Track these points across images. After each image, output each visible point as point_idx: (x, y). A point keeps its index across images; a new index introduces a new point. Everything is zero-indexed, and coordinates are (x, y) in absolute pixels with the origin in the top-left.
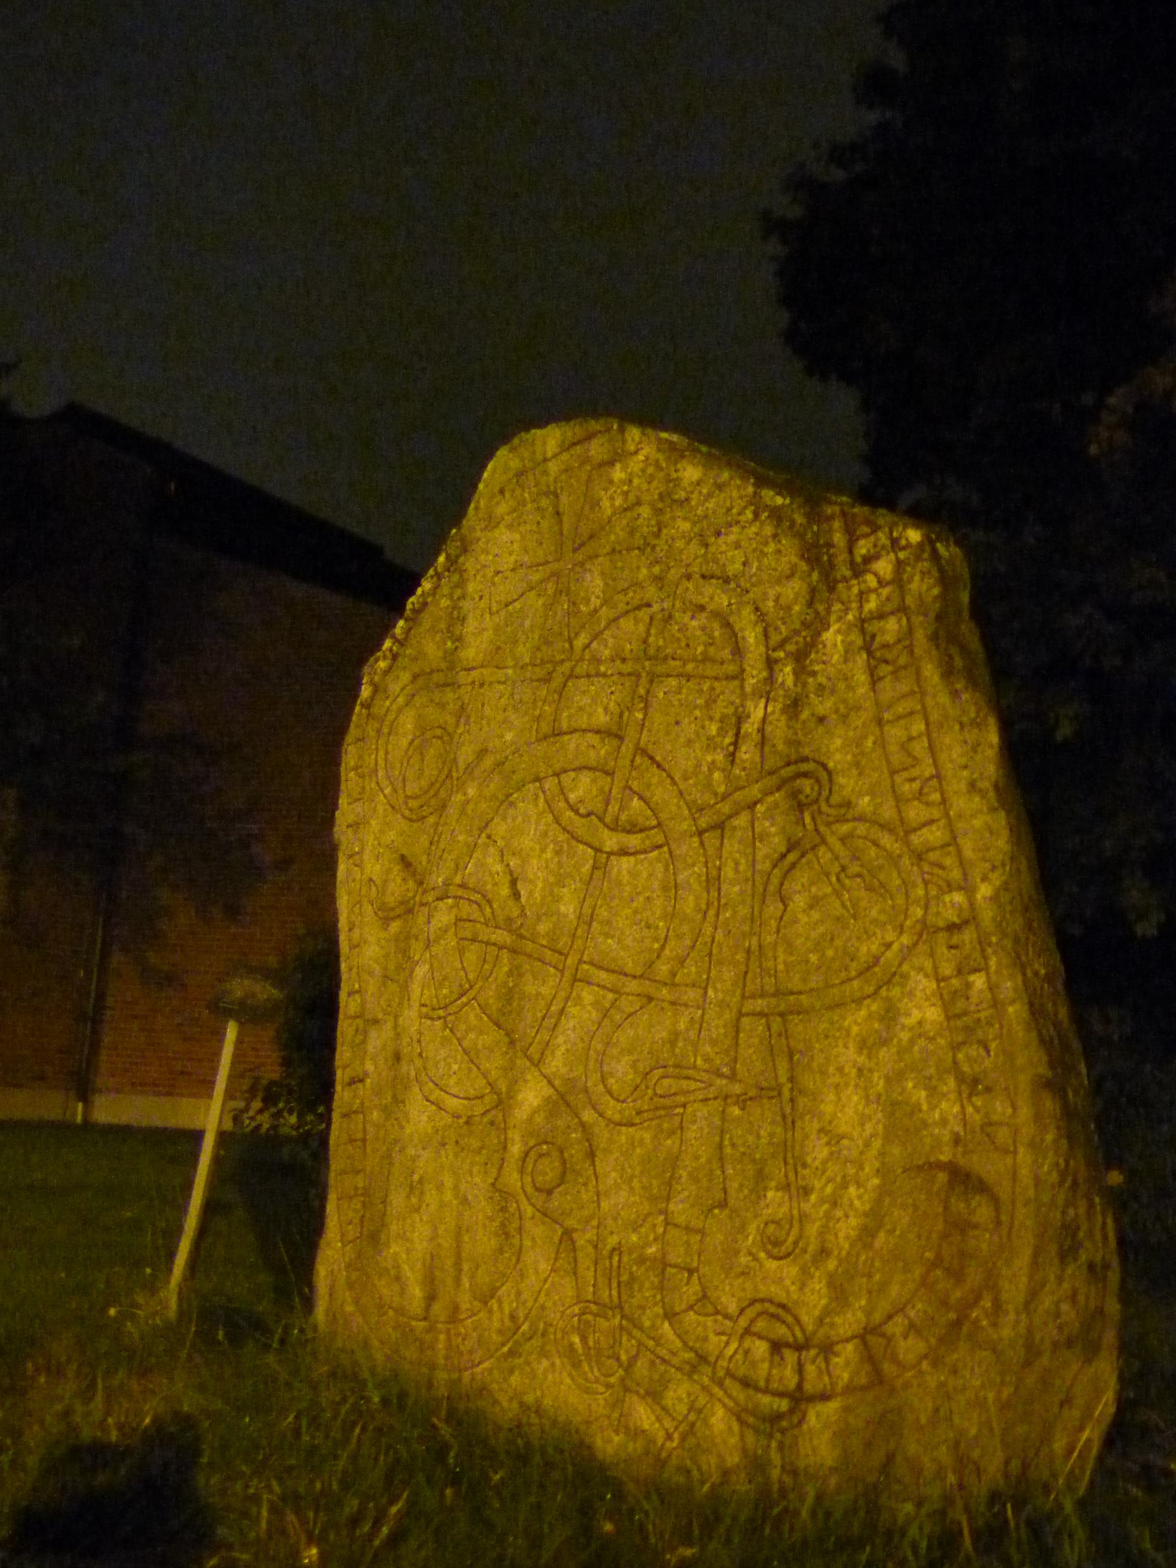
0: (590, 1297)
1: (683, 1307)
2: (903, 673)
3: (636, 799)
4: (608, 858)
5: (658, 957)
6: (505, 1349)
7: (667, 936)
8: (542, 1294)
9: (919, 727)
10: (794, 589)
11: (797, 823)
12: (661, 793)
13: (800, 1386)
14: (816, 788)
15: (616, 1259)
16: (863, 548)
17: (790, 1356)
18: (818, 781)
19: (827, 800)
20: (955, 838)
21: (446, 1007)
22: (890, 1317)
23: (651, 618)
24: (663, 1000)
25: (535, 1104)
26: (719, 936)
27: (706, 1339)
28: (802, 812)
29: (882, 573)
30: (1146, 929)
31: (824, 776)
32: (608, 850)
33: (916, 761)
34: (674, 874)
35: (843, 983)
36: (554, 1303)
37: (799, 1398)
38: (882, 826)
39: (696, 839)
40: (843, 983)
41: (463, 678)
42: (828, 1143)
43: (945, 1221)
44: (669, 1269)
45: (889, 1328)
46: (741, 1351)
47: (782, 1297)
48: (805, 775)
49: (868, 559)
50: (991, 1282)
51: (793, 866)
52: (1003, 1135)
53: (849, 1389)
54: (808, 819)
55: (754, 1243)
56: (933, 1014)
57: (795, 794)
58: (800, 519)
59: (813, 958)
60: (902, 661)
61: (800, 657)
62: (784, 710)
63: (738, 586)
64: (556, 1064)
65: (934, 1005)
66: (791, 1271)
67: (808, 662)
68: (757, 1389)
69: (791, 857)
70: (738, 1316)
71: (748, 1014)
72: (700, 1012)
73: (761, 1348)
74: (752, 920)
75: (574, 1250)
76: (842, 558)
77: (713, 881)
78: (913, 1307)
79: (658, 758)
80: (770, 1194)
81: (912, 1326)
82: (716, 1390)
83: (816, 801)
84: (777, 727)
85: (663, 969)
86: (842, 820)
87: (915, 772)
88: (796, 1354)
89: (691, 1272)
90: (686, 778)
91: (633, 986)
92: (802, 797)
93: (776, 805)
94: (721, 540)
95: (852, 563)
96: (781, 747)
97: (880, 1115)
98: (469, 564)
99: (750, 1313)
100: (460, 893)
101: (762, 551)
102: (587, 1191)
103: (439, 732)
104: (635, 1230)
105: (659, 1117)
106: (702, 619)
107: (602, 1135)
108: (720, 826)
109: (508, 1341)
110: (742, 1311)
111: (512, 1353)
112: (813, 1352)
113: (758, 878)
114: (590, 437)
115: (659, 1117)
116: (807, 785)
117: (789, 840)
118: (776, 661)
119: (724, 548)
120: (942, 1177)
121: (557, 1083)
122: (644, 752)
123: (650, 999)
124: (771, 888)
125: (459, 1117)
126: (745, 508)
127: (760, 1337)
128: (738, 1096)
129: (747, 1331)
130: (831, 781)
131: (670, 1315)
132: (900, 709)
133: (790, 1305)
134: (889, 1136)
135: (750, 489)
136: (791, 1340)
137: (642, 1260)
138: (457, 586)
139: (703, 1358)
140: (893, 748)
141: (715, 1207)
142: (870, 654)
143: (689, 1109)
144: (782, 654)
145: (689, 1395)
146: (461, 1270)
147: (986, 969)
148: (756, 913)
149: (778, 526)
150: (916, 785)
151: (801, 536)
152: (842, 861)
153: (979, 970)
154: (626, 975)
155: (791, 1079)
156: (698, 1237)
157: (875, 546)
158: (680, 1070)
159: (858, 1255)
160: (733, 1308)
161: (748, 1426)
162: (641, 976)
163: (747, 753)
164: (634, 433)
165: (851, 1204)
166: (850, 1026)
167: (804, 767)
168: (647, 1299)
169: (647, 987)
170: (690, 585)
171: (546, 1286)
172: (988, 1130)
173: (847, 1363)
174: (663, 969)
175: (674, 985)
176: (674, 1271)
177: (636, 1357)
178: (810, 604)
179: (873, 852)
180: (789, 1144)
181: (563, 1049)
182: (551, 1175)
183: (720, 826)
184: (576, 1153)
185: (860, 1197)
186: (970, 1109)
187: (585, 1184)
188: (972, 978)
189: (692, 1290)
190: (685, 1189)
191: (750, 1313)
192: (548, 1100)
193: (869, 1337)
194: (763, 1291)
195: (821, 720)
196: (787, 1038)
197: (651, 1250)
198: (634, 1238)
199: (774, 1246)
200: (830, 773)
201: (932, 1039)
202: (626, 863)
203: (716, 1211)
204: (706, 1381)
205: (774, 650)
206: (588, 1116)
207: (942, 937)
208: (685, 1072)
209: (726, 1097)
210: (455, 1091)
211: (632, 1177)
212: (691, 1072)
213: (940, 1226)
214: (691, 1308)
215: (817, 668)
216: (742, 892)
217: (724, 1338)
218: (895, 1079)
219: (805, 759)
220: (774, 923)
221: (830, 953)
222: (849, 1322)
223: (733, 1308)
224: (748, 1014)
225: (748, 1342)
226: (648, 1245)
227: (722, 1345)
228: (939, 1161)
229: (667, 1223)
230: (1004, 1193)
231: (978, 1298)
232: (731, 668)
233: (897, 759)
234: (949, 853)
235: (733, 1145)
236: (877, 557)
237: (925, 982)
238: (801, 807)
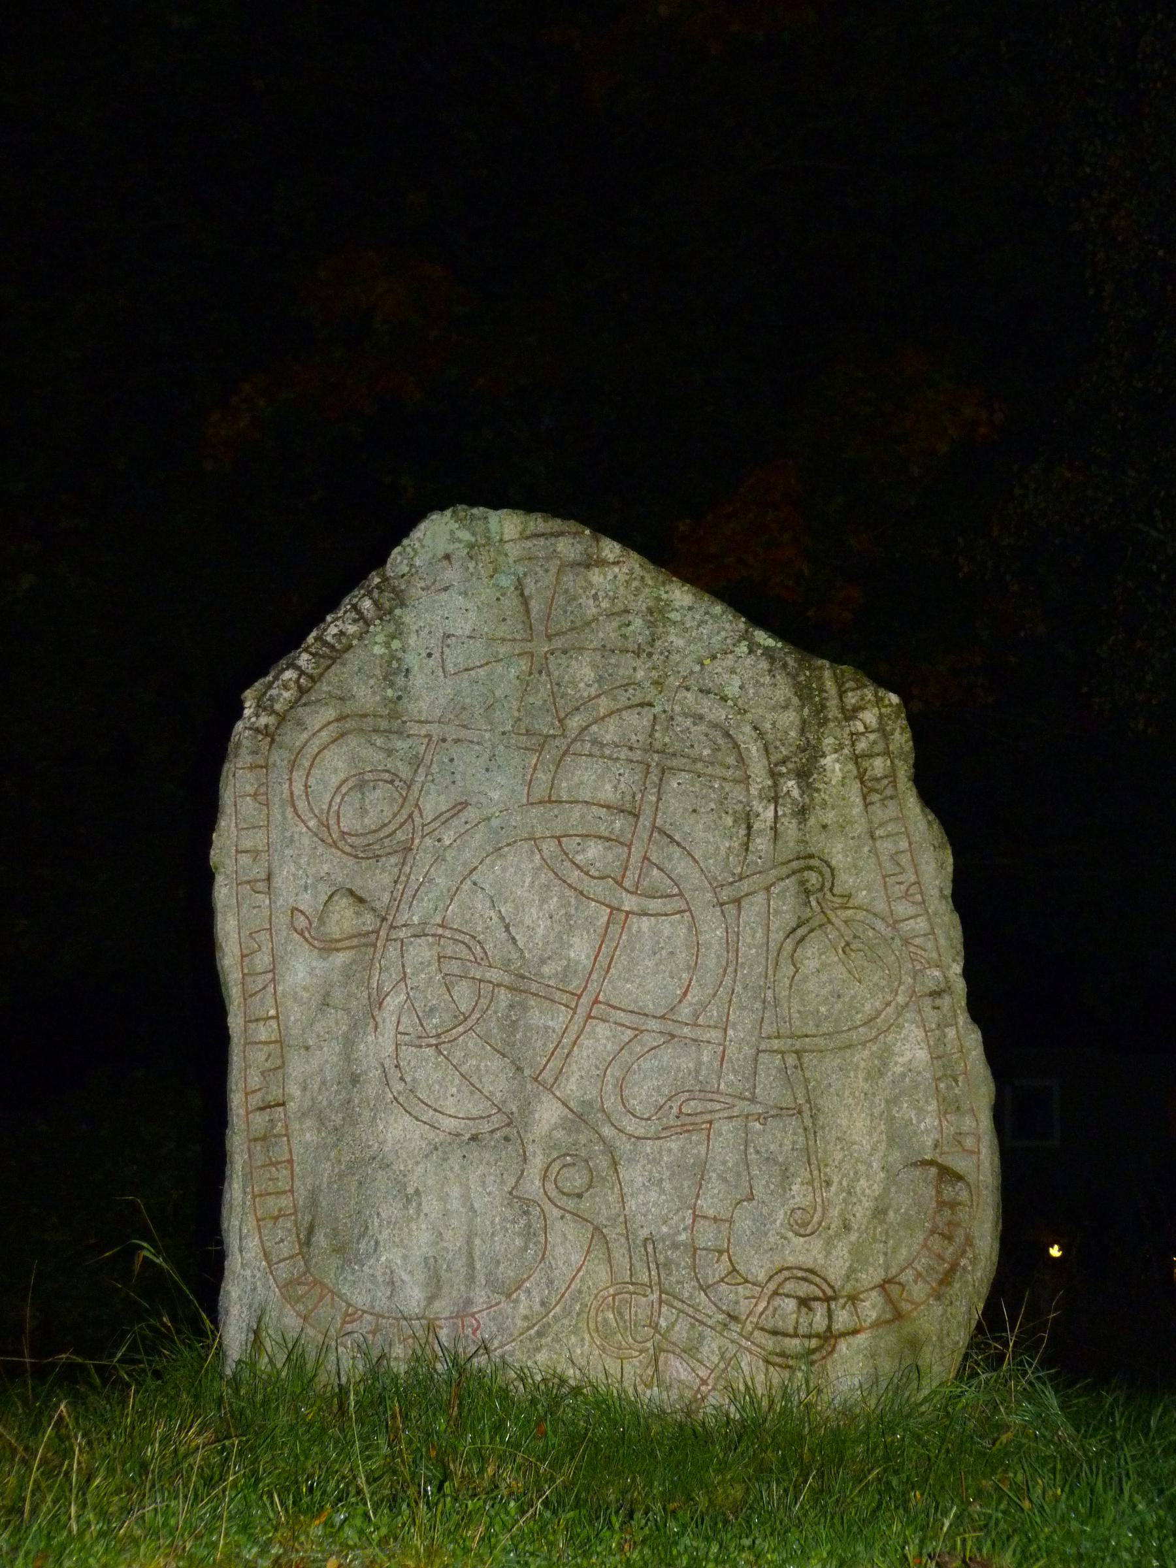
0: (628, 1280)
1: (717, 1278)
2: (888, 803)
3: (655, 869)
4: (627, 917)
5: (680, 1001)
6: (532, 1332)
7: (689, 985)
8: (577, 1280)
9: (904, 845)
10: (790, 718)
11: (805, 904)
12: (681, 866)
13: (829, 1328)
14: (820, 879)
15: (650, 1249)
16: (851, 699)
17: (820, 1309)
18: (821, 873)
19: (831, 890)
20: (933, 929)
21: (438, 1036)
22: (902, 1270)
23: (655, 717)
24: (686, 1038)
25: (553, 1121)
26: (739, 988)
27: (737, 1303)
28: (808, 897)
29: (868, 722)
31: (826, 871)
32: (627, 909)
33: (903, 871)
34: (696, 935)
35: (850, 1029)
36: (589, 1288)
37: (829, 1337)
38: (875, 915)
39: (718, 909)
40: (850, 1029)
41: (414, 729)
42: (842, 1149)
43: (937, 1201)
44: (699, 1251)
45: (903, 1278)
46: (771, 1308)
47: (810, 1264)
48: (810, 868)
49: (857, 709)
50: (969, 1241)
51: (803, 939)
52: (969, 1142)
53: (876, 1325)
54: (814, 903)
55: (782, 1225)
56: (922, 1055)
57: (802, 883)
58: (791, 662)
59: (823, 1009)
60: (889, 792)
61: (803, 775)
62: (794, 814)
63: (735, 705)
64: (571, 1087)
65: (922, 1049)
66: (817, 1244)
67: (811, 780)
68: (786, 1335)
69: (800, 932)
70: (767, 1283)
72: (721, 1048)
73: (791, 1305)
74: (766, 977)
75: (607, 1243)
76: (833, 704)
77: (731, 945)
78: (919, 1261)
79: (677, 838)
80: (794, 1187)
81: (919, 1275)
82: (743, 1342)
83: (821, 889)
84: (788, 828)
85: (685, 1011)
86: (845, 907)
87: (901, 878)
88: (825, 1305)
89: (721, 1252)
90: (706, 859)
91: (653, 1024)
92: (808, 885)
93: (787, 889)
94: (717, 662)
95: (843, 709)
96: (791, 844)
97: (883, 1127)
98: (408, 617)
99: (779, 1279)
100: (440, 931)
101: (757, 681)
102: (613, 1193)
103: (387, 776)
104: (665, 1222)
105: (688, 1131)
106: (702, 728)
107: (624, 1146)
109: (534, 1325)
110: (771, 1278)
111: (540, 1334)
112: (842, 1301)
113: (772, 944)
114: (561, 534)
115: (688, 1131)
116: (813, 878)
117: (799, 917)
118: (781, 775)
119: (719, 670)
120: (933, 1170)
121: (572, 1104)
122: (662, 832)
123: (673, 1036)
124: (785, 954)
125: (458, 1135)
126: (739, 641)
127: (788, 1296)
128: (760, 1114)
129: (776, 1293)
130: (833, 875)
131: (704, 1289)
132: (890, 828)
133: (817, 1268)
134: (892, 1141)
135: (742, 626)
136: (821, 1295)
137: (675, 1246)
138: (393, 637)
139: (734, 1318)
140: (884, 858)
141: (744, 1201)
142: (862, 783)
144: (784, 770)
145: (720, 1348)
146: (474, 1269)
147: (956, 1024)
149: (772, 664)
150: (903, 887)
151: (794, 677)
152: (846, 938)
153: (952, 1025)
154: (646, 1015)
155: (808, 1101)
156: (727, 1225)
157: (862, 699)
158: (705, 1093)
159: (875, 1228)
160: (762, 1277)
161: (774, 1365)
162: (663, 1017)
163: (761, 843)
164: (610, 549)
165: (863, 1193)
166: (858, 1062)
167: (813, 862)
168: (683, 1275)
169: (670, 1027)
170: (689, 695)
171: (581, 1273)
172: (958, 1138)
173: (874, 1306)
174: (685, 1011)
175: (696, 1025)
176: (704, 1252)
177: (673, 1324)
178: (802, 732)
179: (871, 933)
180: (811, 1150)
181: (577, 1076)
182: (579, 1181)
183: (737, 901)
184: (602, 1162)
185: (870, 1187)
186: (945, 1123)
187: (612, 1188)
188: (947, 1030)
189: (724, 1266)
190: (714, 1186)
191: (779, 1279)
192: (565, 1119)
193: (887, 1286)
194: (791, 1260)
195: (824, 827)
196: (802, 1070)
197: (683, 1237)
198: (665, 1229)
199: (801, 1226)
200: (832, 870)
201: (919, 1073)
202: (645, 923)
203: (745, 1203)
204: (735, 1336)
205: (776, 765)
206: (607, 1131)
207: (928, 1001)
208: (710, 1096)
209: (747, 1116)
210: (452, 1112)
211: (661, 1180)
212: (715, 1096)
213: (934, 1205)
214: (722, 1280)
215: (821, 786)
216: (758, 955)
217: (754, 1301)
218: (892, 1102)
219: (811, 856)
220: (787, 982)
221: (839, 1006)
222: (871, 1276)
223: (762, 1277)
225: (777, 1301)
226: (679, 1233)
227: (752, 1306)
228: (924, 1159)
229: (695, 1217)
230: (971, 1179)
231: (964, 1252)
232: (739, 774)
233: (889, 866)
234: (929, 940)
235: (758, 1152)
236: (863, 708)
237: (916, 1030)
238: (808, 893)
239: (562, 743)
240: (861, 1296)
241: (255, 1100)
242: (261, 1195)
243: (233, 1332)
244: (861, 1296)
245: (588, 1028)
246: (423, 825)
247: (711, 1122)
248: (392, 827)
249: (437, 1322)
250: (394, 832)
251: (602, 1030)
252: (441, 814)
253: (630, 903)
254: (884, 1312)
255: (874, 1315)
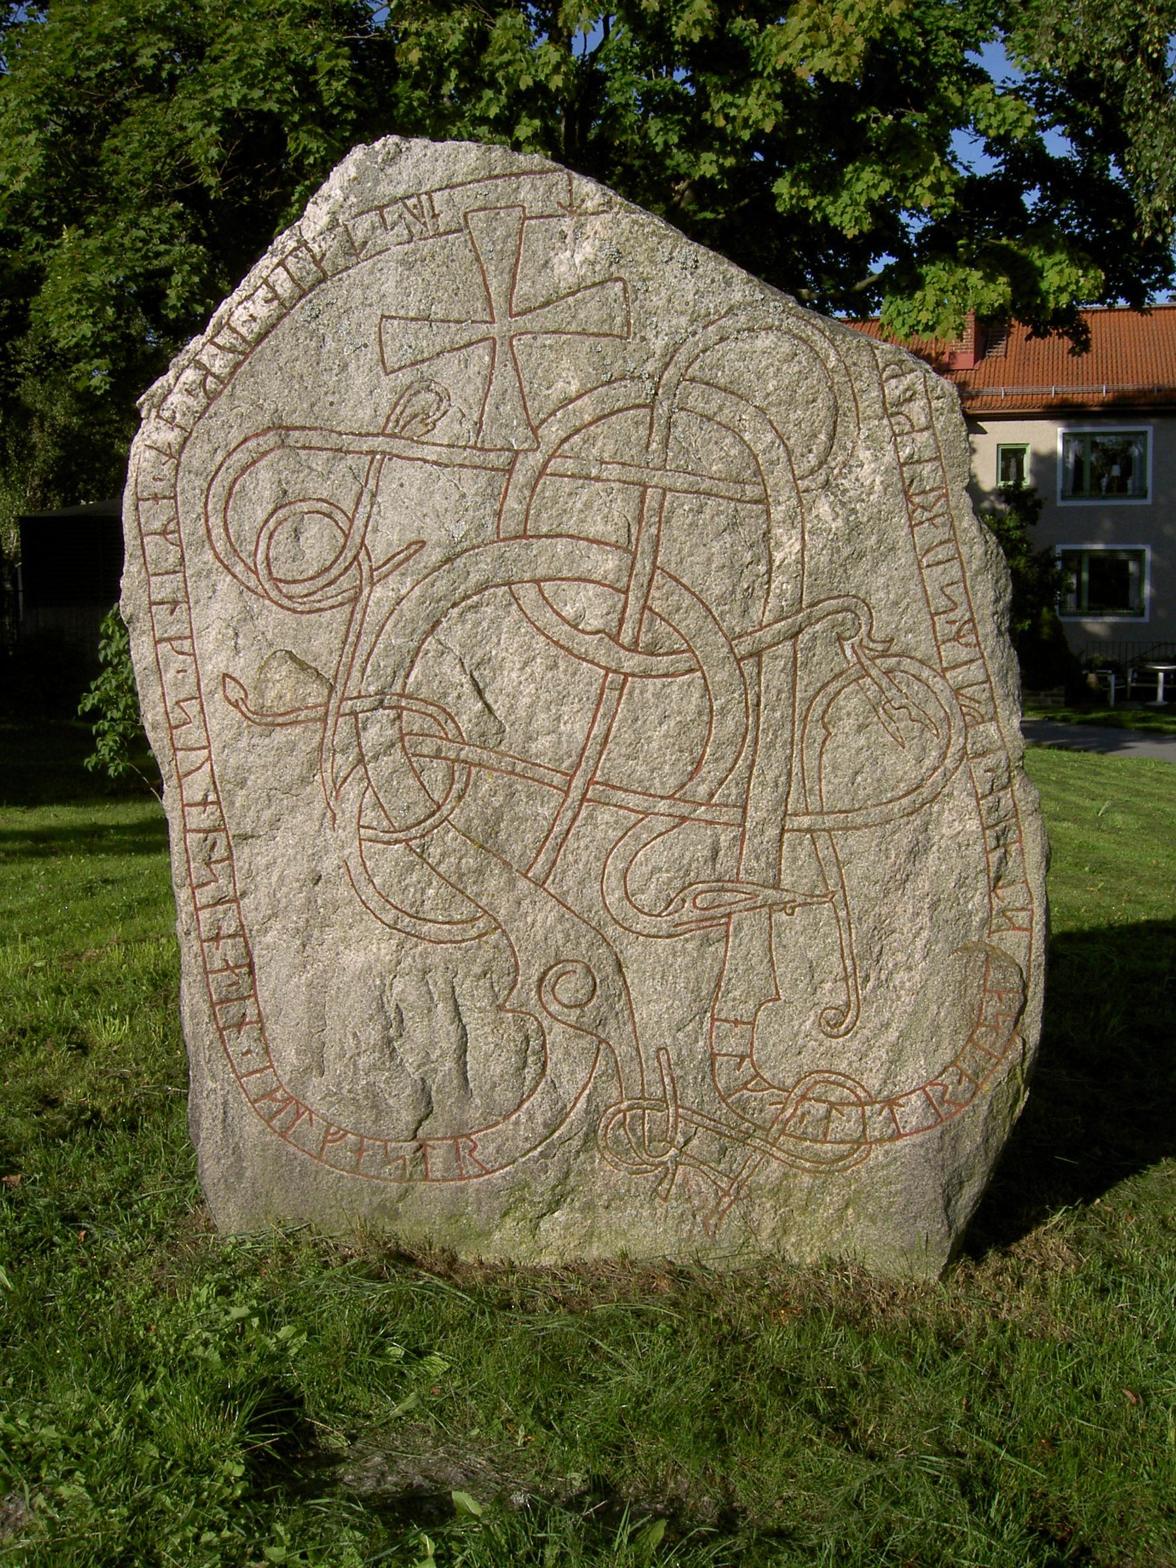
6: (536, 1153)
9: (955, 571)
30: (892, 261)
48: (847, 610)
54: (849, 652)
71: (204, 907)
86: (884, 654)
87: (952, 617)
91: (662, 806)
107: (631, 951)
108: (757, 654)
129: (804, 1097)
142: (908, 498)
143: (735, 917)
148: (796, 738)
150: (955, 628)
183: (757, 654)
224: (204, 907)
239: (538, 458)
240: (901, 1101)
241: (204, 896)
242: (221, 1002)
243: (231, 1207)
244: (901, 1101)
245: (583, 814)
246: (372, 570)
247: (729, 915)
248: (334, 572)
249: (431, 1143)
250: (337, 578)
251: (605, 816)
252: (394, 556)
253: (631, 663)
254: (925, 1117)
255: (914, 1121)
